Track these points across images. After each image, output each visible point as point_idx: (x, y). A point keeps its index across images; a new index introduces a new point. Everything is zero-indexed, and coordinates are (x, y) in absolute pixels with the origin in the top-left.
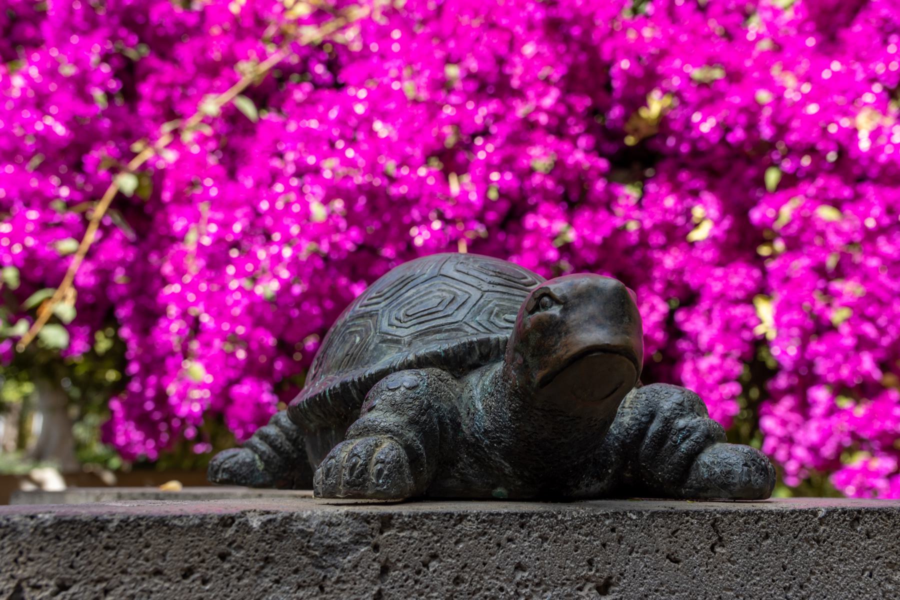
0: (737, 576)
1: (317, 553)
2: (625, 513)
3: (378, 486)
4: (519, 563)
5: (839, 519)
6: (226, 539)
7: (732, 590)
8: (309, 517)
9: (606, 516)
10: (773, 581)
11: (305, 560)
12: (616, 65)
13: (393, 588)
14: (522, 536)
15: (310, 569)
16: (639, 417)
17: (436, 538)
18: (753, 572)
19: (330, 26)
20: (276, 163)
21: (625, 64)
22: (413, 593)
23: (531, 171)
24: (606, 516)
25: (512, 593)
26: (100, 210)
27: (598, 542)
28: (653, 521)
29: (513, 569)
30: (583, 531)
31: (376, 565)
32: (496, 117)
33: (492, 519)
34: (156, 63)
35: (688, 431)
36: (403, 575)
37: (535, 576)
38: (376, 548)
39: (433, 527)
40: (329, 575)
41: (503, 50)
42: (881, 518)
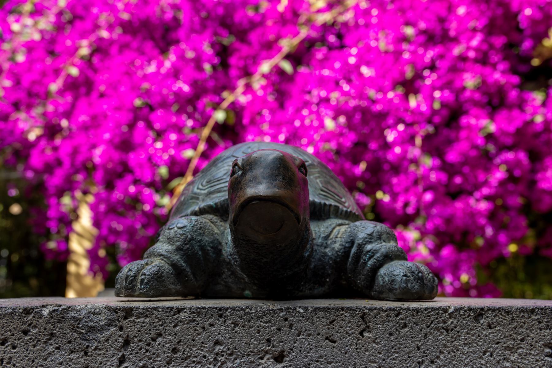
0: (380, 353)
1: (83, 331)
2: (295, 308)
3: (141, 289)
4: (217, 340)
5: (464, 315)
6: (27, 322)
7: (376, 363)
8: (82, 309)
9: (281, 310)
10: (409, 357)
11: (76, 335)
12: (522, 13)
13: (131, 354)
14: (220, 323)
15: (78, 341)
16: (344, 244)
17: (161, 323)
18: (393, 350)
19: (335, 12)
20: (307, 97)
21: (528, 12)
22: (144, 357)
23: (464, 89)
24: (281, 310)
25: (212, 360)
26: (206, 132)
27: (274, 328)
28: (316, 314)
29: (212, 344)
30: (263, 320)
31: (121, 340)
32: (441, 57)
33: (199, 311)
34: (238, 45)
35: (373, 253)
36: (138, 346)
37: (229, 349)
38: (121, 329)
39: (159, 316)
40: (90, 345)
41: (443, 12)
42: (501, 314)
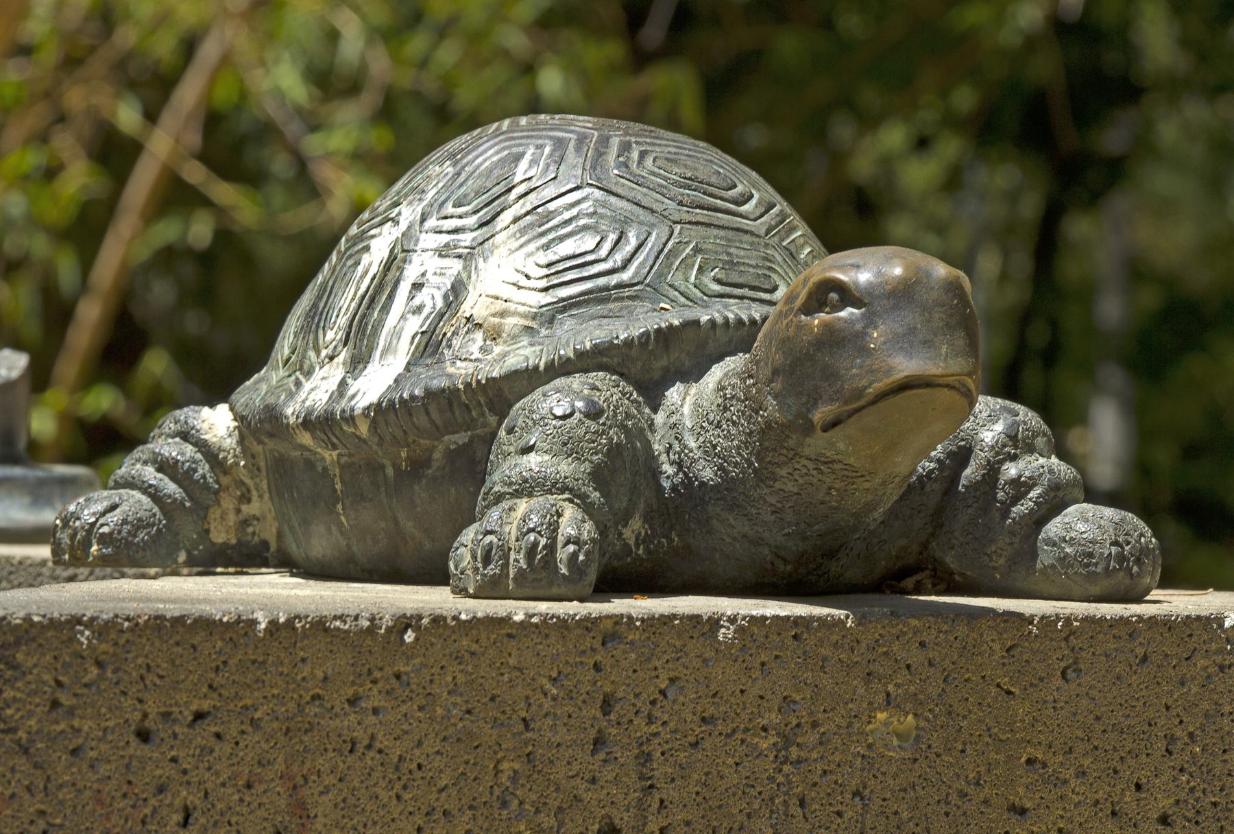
35: (1020, 487)
